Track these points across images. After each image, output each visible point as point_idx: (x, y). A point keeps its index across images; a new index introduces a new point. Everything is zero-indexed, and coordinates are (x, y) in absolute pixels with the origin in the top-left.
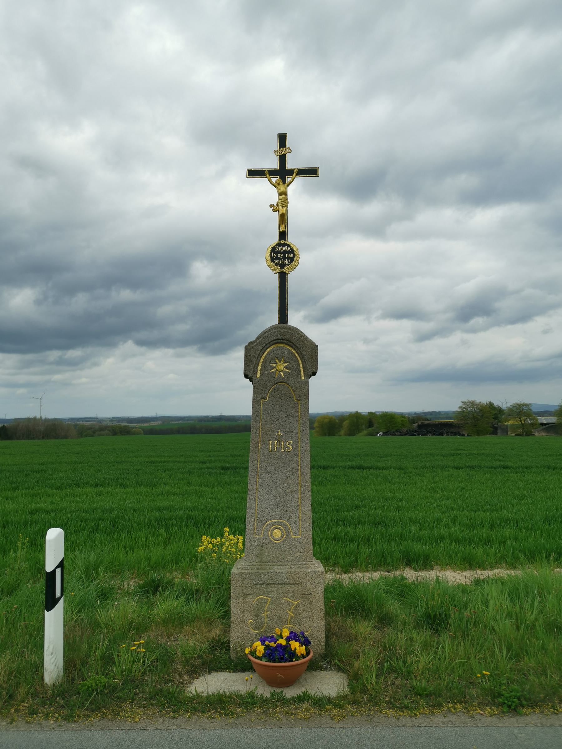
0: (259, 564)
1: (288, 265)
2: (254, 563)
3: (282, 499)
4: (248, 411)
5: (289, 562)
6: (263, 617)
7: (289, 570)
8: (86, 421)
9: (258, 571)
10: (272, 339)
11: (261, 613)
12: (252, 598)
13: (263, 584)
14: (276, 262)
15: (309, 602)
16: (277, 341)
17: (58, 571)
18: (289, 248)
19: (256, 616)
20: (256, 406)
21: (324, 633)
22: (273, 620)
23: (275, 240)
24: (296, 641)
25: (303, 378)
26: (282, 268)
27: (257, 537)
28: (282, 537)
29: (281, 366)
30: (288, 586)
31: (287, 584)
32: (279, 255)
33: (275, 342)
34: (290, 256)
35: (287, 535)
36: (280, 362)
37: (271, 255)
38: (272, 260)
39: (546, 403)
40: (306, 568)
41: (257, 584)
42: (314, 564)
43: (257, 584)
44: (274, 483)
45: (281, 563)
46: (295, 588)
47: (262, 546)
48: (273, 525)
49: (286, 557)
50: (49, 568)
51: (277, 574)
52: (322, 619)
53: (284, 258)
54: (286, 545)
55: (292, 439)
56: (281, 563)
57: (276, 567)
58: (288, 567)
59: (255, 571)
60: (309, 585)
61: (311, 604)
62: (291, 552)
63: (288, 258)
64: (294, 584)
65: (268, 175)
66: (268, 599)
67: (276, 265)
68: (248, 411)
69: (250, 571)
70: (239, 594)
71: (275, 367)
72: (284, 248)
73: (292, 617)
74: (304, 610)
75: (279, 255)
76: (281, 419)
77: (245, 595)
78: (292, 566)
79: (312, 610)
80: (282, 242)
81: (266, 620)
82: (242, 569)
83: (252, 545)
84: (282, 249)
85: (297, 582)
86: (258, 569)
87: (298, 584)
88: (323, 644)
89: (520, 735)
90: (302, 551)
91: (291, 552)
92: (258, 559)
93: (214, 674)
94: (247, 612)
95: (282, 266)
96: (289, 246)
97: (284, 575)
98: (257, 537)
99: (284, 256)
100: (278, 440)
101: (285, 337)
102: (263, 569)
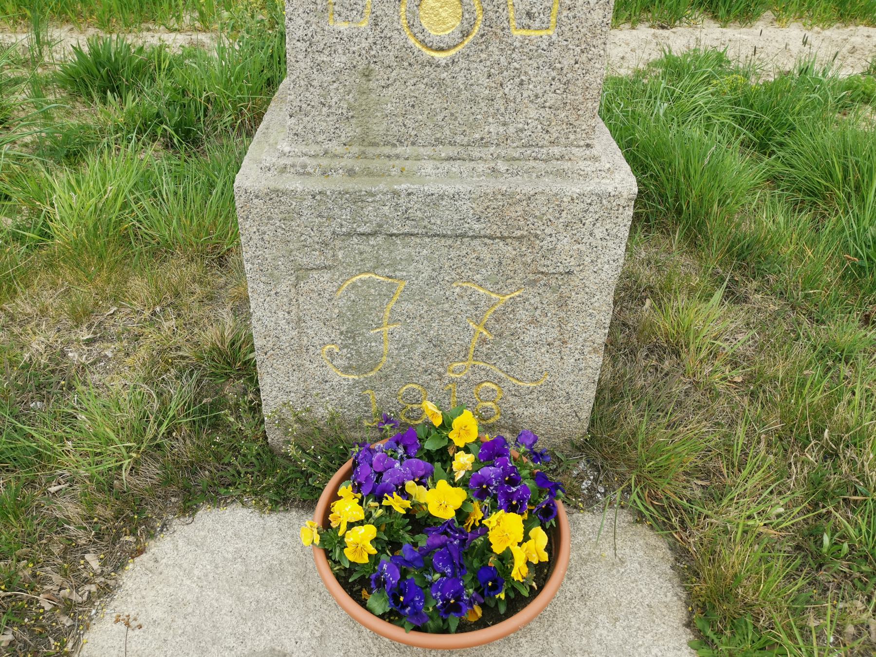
0: (355, 149)
2: (335, 147)
4: (547, 560)
5: (486, 145)
6: (378, 339)
7: (490, 185)
9: (352, 185)
11: (370, 328)
12: (331, 280)
13: (374, 234)
15: (556, 296)
19: (351, 335)
20: (502, 609)
21: (593, 388)
22: (413, 346)
24: (511, 509)
27: (343, 26)
28: (465, 34)
30: (477, 242)
31: (474, 237)
35: (488, 24)
40: (561, 174)
41: (349, 235)
42: (595, 159)
43: (349, 235)
45: (451, 151)
46: (509, 251)
47: (367, 75)
49: (474, 125)
51: (434, 201)
52: (595, 351)
54: (479, 75)
56: (451, 151)
57: (429, 167)
58: (481, 167)
59: (337, 183)
60: (565, 242)
61: (562, 303)
62: (499, 104)
64: (503, 238)
66: (392, 285)
68: (547, 560)
69: (315, 184)
70: (276, 268)
73: (484, 341)
74: (534, 321)
77: (301, 272)
78: (502, 166)
79: (561, 323)
81: (386, 347)
82: (283, 170)
83: (319, 67)
85: (519, 233)
86: (351, 173)
87: (520, 239)
88: (585, 415)
90: (551, 99)
91: (499, 104)
92: (350, 130)
93: (208, 518)
94: (316, 325)
97: (465, 206)
98: (343, 26)
102: (370, 173)
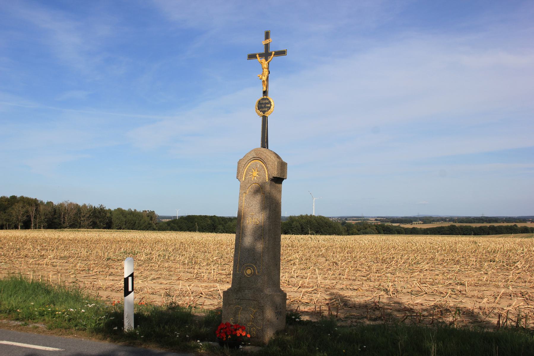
8: (353, 220)
16: (255, 158)
17: (130, 279)
23: (261, 96)
26: (264, 113)
34: (269, 105)
50: (126, 276)
53: (265, 107)
63: (267, 107)
80: (265, 97)
84: (264, 102)
95: (264, 112)
96: (268, 99)
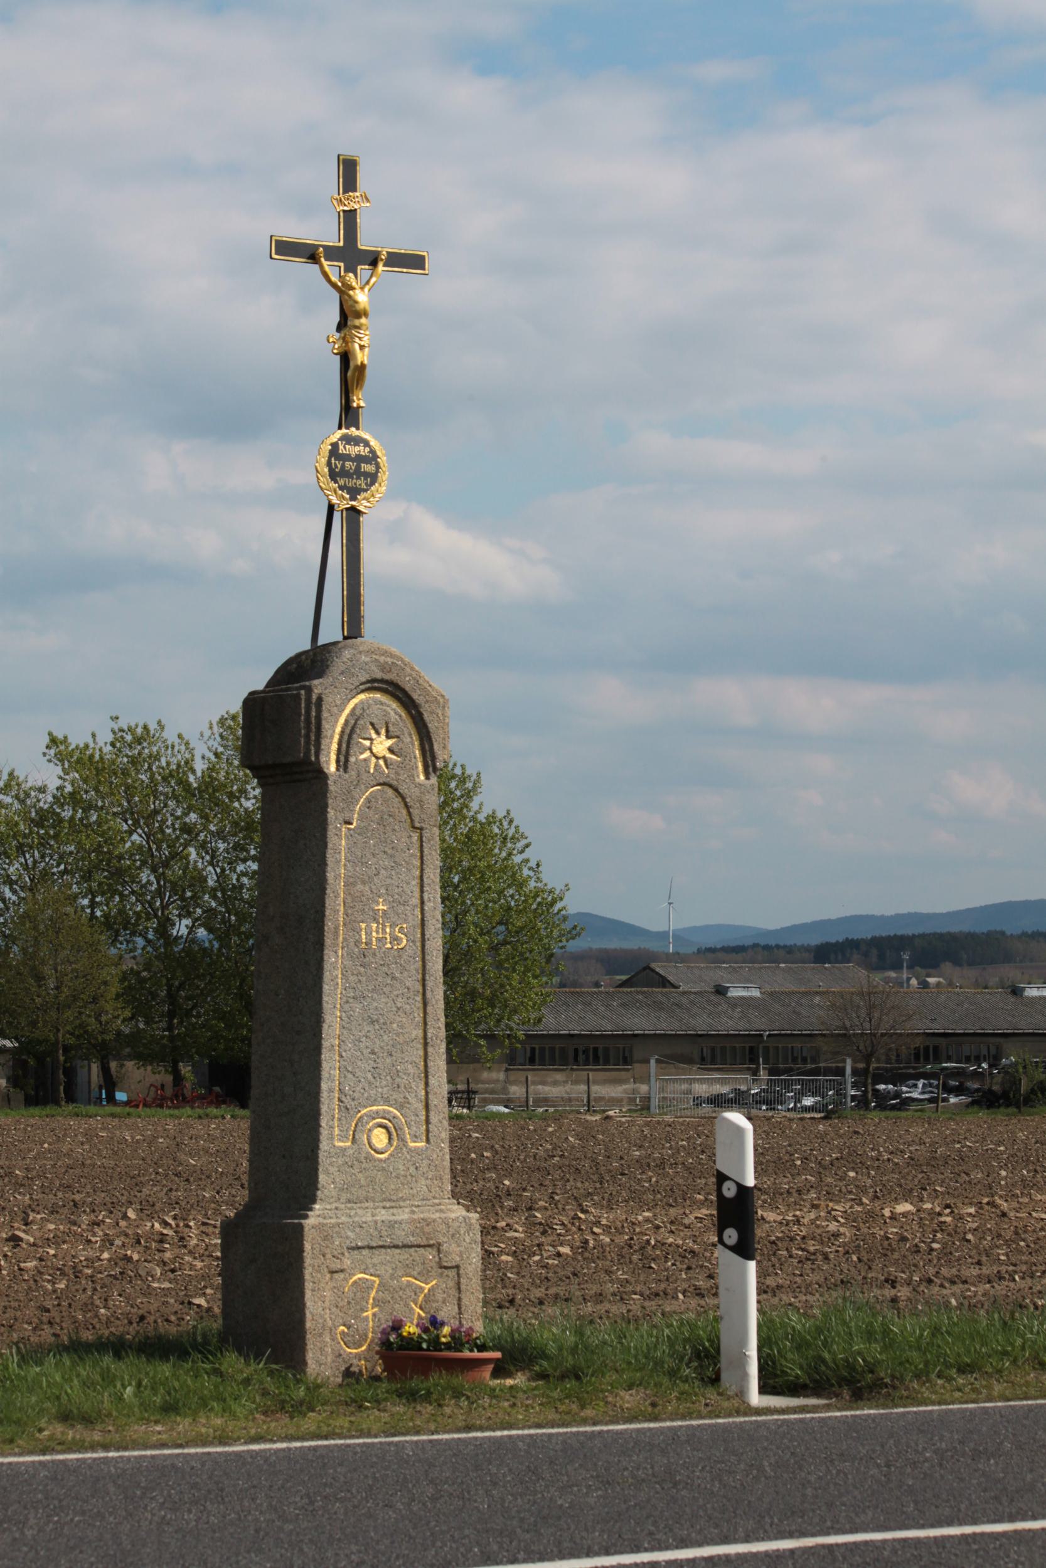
1: (366, 491)
3: (388, 1060)
10: (363, 680)
14: (342, 482)
18: (367, 449)
25: (422, 777)
29: (382, 745)
32: (348, 464)
33: (369, 685)
36: (378, 733)
37: (329, 464)
38: (333, 476)
39: (738, 922)
44: (373, 1022)
48: (374, 1118)
53: (358, 473)
55: (406, 921)
57: (383, 1212)
60: (454, 1247)
63: (366, 475)
65: (63, 1103)
67: (341, 488)
71: (371, 740)
72: (357, 448)
75: (348, 464)
76: (383, 872)
89: (99, 1276)
99: (358, 467)
100: (378, 923)
101: (387, 677)
